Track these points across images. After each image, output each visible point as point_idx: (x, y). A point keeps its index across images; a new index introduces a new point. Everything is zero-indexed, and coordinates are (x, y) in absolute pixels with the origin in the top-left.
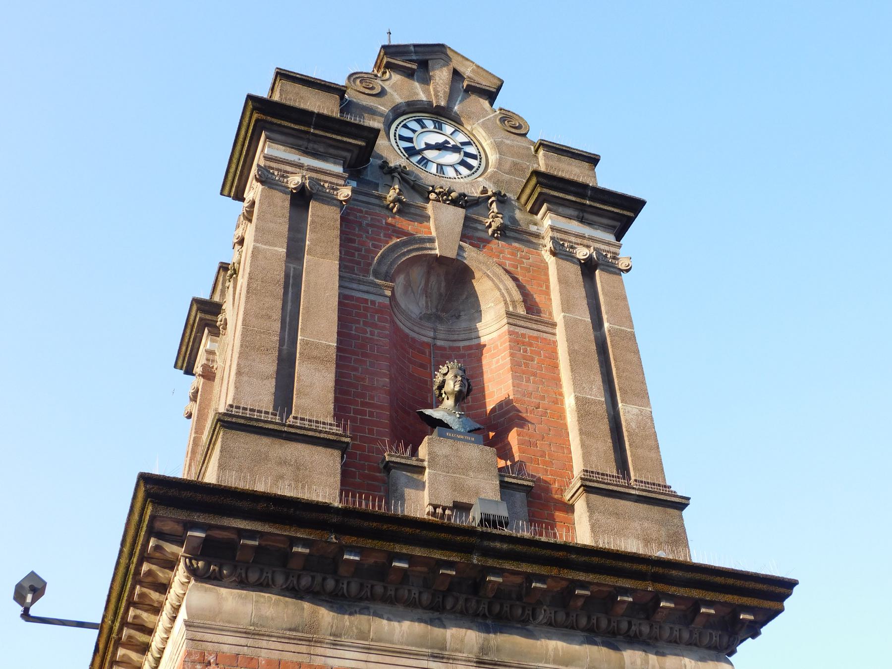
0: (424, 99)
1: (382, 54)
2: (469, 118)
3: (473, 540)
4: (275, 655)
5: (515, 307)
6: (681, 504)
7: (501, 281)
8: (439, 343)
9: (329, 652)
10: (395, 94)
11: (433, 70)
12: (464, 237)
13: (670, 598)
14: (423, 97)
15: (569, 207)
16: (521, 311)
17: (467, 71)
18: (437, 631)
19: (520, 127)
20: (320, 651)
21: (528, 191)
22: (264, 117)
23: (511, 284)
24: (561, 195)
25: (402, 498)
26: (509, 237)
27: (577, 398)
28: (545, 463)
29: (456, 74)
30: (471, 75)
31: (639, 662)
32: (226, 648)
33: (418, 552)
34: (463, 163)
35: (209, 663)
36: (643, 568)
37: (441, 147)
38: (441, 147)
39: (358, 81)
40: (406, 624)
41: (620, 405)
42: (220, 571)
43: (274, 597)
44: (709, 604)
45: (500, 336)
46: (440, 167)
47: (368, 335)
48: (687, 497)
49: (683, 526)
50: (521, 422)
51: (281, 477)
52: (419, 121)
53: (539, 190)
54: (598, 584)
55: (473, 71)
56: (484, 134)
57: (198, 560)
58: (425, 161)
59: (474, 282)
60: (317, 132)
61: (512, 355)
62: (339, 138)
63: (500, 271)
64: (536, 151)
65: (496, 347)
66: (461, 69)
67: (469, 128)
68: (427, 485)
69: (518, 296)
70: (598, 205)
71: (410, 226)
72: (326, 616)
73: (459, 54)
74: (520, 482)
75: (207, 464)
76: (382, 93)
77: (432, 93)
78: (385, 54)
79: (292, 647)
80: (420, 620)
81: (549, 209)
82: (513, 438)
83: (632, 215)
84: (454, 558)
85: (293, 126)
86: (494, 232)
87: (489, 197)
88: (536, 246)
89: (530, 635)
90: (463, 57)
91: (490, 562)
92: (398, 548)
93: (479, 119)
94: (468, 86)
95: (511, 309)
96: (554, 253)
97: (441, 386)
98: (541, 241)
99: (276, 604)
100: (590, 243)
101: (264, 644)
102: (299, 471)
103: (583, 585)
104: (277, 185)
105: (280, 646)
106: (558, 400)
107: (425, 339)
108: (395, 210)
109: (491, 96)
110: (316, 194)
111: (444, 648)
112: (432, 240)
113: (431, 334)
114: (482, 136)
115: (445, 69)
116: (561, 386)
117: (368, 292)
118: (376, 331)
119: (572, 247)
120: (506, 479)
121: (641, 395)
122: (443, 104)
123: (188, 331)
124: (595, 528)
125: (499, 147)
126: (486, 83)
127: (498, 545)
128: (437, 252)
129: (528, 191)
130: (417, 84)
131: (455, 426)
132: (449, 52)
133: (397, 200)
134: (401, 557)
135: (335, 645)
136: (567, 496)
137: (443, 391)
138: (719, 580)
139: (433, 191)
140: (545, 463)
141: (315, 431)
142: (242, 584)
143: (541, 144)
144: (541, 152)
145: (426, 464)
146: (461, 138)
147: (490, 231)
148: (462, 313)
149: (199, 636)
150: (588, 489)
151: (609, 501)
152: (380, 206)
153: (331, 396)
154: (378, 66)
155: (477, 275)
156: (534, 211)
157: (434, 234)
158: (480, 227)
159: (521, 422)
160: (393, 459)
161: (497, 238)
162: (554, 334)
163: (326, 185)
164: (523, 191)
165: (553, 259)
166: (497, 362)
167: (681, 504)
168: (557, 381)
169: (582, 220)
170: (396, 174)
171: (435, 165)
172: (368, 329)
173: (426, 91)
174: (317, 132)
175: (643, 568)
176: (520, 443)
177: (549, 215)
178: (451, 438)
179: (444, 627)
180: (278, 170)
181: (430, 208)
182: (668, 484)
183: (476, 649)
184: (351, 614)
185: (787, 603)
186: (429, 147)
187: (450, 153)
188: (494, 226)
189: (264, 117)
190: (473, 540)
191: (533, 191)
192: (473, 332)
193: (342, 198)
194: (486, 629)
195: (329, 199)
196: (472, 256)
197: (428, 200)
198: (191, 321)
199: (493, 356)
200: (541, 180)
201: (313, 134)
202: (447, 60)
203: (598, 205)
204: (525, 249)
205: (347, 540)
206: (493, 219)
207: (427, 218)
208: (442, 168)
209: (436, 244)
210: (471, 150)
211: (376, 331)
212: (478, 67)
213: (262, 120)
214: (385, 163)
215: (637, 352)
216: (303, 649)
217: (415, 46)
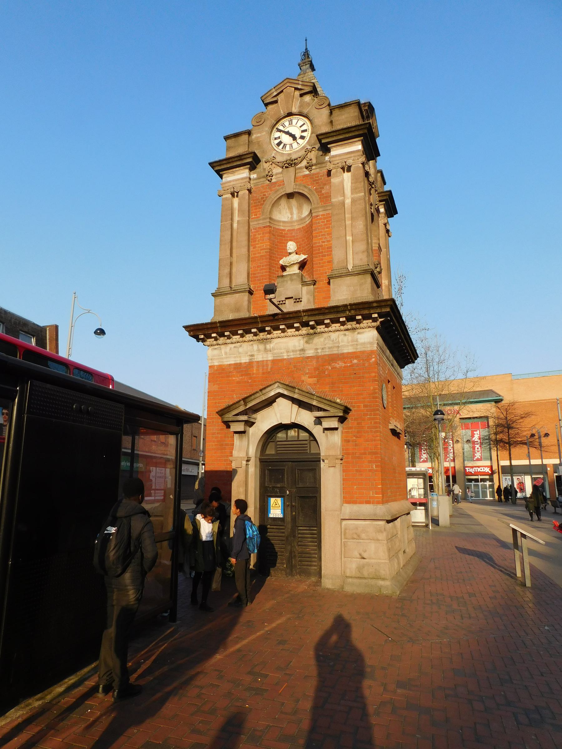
1: (367, 104)
53: (388, 198)
81: (384, 204)
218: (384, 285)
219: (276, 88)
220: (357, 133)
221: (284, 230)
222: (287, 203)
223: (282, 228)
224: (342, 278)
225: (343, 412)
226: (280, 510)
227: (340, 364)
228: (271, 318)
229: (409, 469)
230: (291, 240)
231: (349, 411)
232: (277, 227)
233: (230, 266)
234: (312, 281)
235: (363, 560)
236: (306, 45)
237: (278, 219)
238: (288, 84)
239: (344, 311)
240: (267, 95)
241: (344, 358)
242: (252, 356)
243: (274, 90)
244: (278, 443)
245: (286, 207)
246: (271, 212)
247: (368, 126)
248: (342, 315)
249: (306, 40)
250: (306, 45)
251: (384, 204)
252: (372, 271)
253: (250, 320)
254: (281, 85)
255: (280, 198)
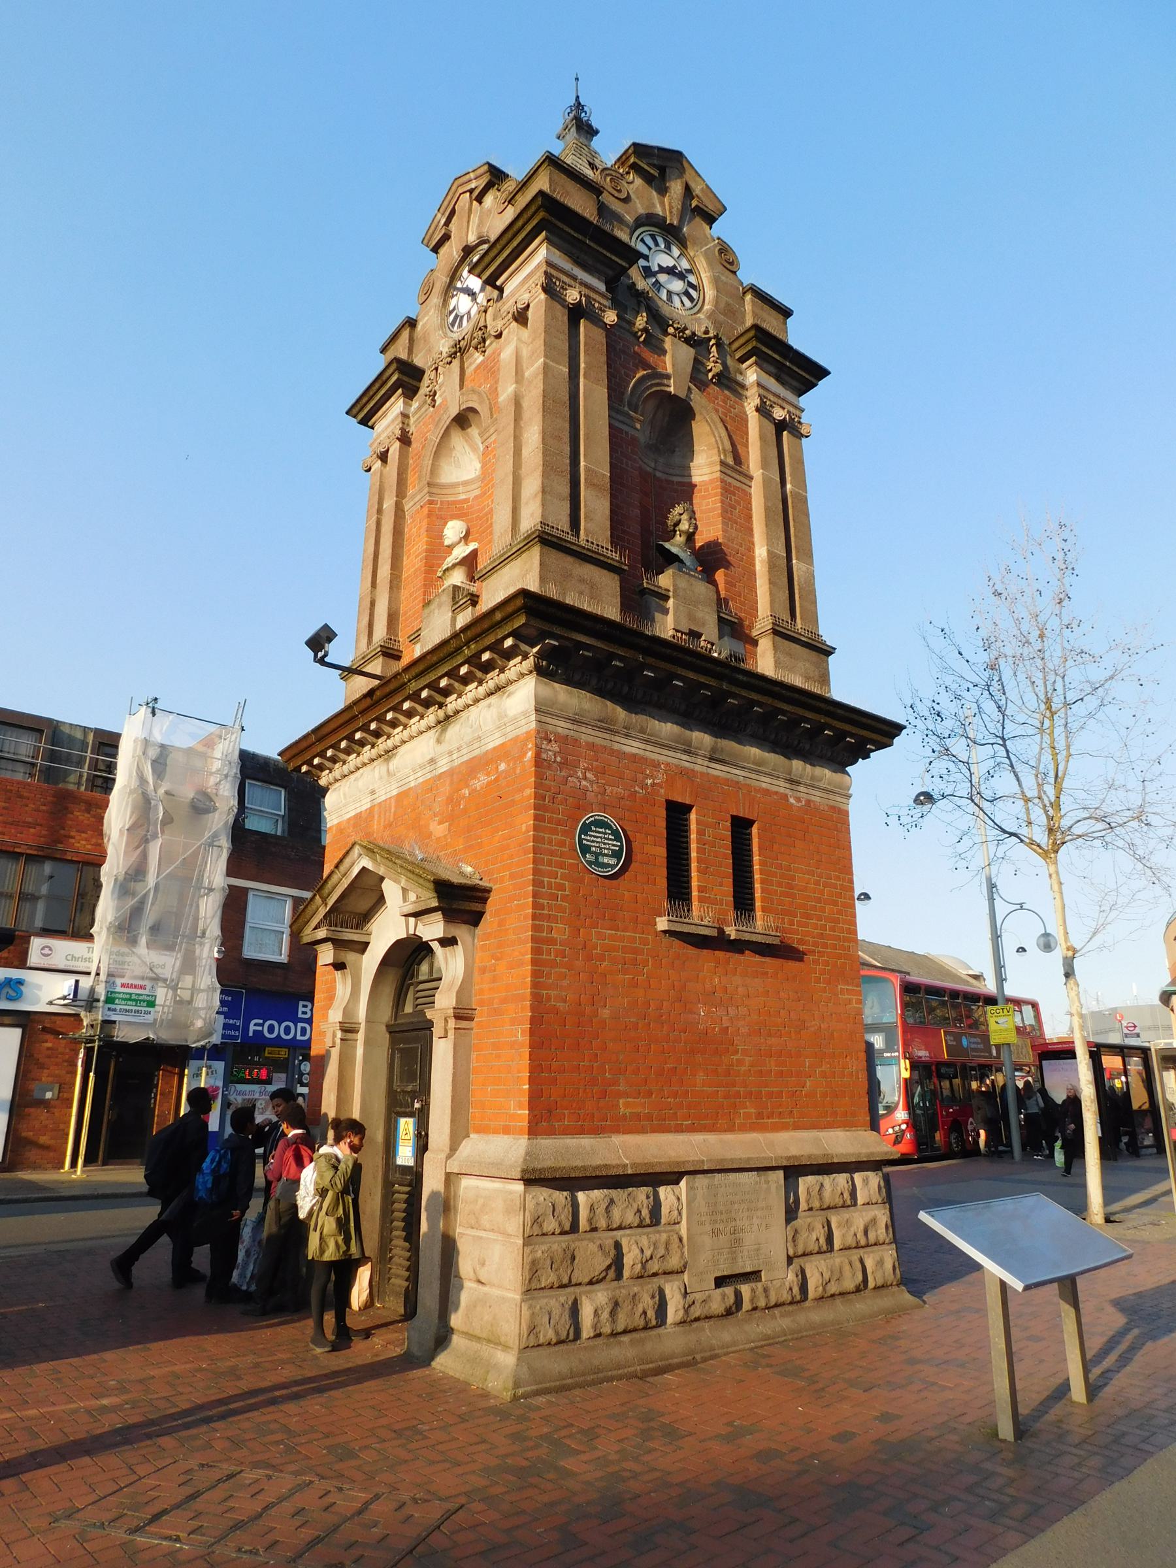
0: (661, 213)
1: (630, 151)
2: (694, 244)
3: (727, 671)
4: (591, 739)
5: (725, 456)
6: (828, 652)
7: (717, 428)
8: (658, 474)
9: (623, 741)
10: (637, 201)
11: (670, 181)
12: (693, 379)
13: (831, 728)
14: (659, 210)
15: (771, 364)
16: (730, 461)
17: (697, 189)
18: (688, 733)
19: (732, 263)
20: (617, 739)
21: (742, 340)
22: (550, 218)
23: (724, 434)
24: (770, 352)
25: (653, 620)
26: (722, 384)
27: (769, 552)
28: (741, 602)
29: (688, 189)
30: (700, 194)
31: (800, 769)
32: (560, 730)
33: (691, 675)
34: (687, 294)
35: (551, 741)
36: (822, 705)
37: (671, 271)
38: (671, 271)
39: (608, 179)
40: (669, 724)
41: (794, 561)
42: (557, 671)
43: (588, 694)
44: (852, 735)
45: (711, 481)
46: (669, 293)
47: (624, 466)
48: (562, 551)
49: (828, 669)
50: (727, 565)
51: (581, 593)
52: (653, 238)
53: (754, 343)
54: (792, 713)
55: (702, 190)
56: (705, 265)
57: (543, 660)
58: (658, 285)
59: (694, 424)
60: (592, 244)
61: (722, 502)
62: (608, 255)
63: (717, 420)
64: (744, 293)
65: (706, 490)
66: (692, 185)
67: (692, 254)
68: (671, 611)
69: (728, 446)
70: (795, 368)
71: (652, 359)
72: (621, 713)
73: (693, 168)
74: (729, 618)
75: (379, 523)
76: (627, 200)
77: (667, 207)
78: (634, 152)
79: (600, 734)
80: (677, 724)
81: (756, 363)
82: (720, 576)
83: (627, 266)
84: (712, 682)
85: (572, 232)
86: (713, 377)
87: (710, 339)
88: (740, 396)
89: (740, 742)
90: (697, 172)
91: (734, 689)
92: (680, 671)
93: (701, 248)
94: (697, 206)
95: (722, 457)
96: (757, 410)
97: (677, 523)
98: (745, 393)
99: (570, 693)
100: (785, 405)
101: (583, 730)
102: (594, 592)
103: (784, 712)
104: (557, 296)
105: (593, 732)
106: (750, 548)
107: (648, 469)
108: (642, 339)
109: (710, 219)
110: (588, 313)
111: (690, 746)
112: (668, 377)
113: (653, 465)
114: (702, 265)
115: (679, 181)
116: (752, 536)
117: (623, 423)
118: (630, 462)
119: (771, 406)
120: (721, 615)
121: (808, 556)
122: (675, 223)
123: (377, 385)
124: (777, 664)
125: (716, 282)
126: (710, 206)
127: (741, 677)
128: (672, 389)
129: (742, 340)
130: (654, 193)
131: (688, 564)
132: (685, 163)
133: (645, 330)
134: (680, 678)
135: (627, 736)
136: (754, 633)
137: (677, 529)
138: (864, 720)
139: (672, 326)
140: (741, 602)
141: (605, 556)
142: (568, 681)
143: (751, 288)
144: (749, 297)
145: (671, 594)
146: (684, 265)
147: (710, 375)
148: (677, 449)
149: (544, 719)
150: (776, 632)
151: (787, 643)
152: (628, 331)
153: (608, 523)
154: (622, 160)
155: (697, 417)
156: (742, 360)
157: (670, 370)
158: (702, 369)
159: (727, 565)
160: (649, 586)
161: (714, 383)
162: (750, 487)
163: (596, 305)
164: (737, 338)
165: (755, 413)
166: (708, 504)
167: (828, 652)
168: (750, 530)
169: (778, 379)
170: (642, 299)
171: (665, 291)
172: (625, 461)
173: (662, 204)
174: (592, 244)
175: (822, 705)
176: (726, 582)
177: (755, 368)
178: (686, 573)
179: (691, 730)
180: (599, 303)
181: (668, 342)
182: (820, 633)
183: (709, 749)
184: (636, 714)
185: (896, 740)
186: (662, 270)
187: (676, 279)
188: (715, 371)
189: (550, 218)
190: (727, 671)
191: (747, 342)
192: (686, 470)
193: (608, 322)
194: (715, 735)
195: (597, 321)
196: (698, 400)
197: (666, 334)
198: (384, 377)
199: (704, 497)
200: (759, 334)
201: (589, 246)
202: (682, 171)
203: (795, 368)
204: (733, 398)
205: (651, 660)
206: (713, 366)
207: (664, 352)
208: (671, 296)
209: (672, 381)
210: (692, 279)
211: (630, 462)
212: (707, 186)
213: (548, 221)
214: (634, 284)
215: (808, 515)
216: (607, 736)
217: (660, 149)
218: (760, 561)
219: (441, 210)
220: (529, 228)
221: (466, 501)
222: (466, 441)
223: (463, 497)
224: (499, 572)
225: (438, 897)
226: (411, 1149)
227: (481, 781)
228: (368, 701)
229: (1166, 1044)
230: (453, 518)
231: (486, 895)
232: (451, 499)
233: (370, 609)
234: (466, 596)
235: (480, 1287)
236: (577, 90)
237: (456, 481)
238: (460, 191)
239: (458, 650)
240: (431, 231)
241: (487, 763)
242: (373, 792)
243: (439, 215)
244: (421, 987)
245: (467, 448)
246: (434, 470)
247: (539, 201)
248: (460, 660)
249: (577, 79)
250: (577, 90)
251: (756, 363)
252: (538, 536)
253: (345, 714)
254: (449, 197)
255: (447, 433)
